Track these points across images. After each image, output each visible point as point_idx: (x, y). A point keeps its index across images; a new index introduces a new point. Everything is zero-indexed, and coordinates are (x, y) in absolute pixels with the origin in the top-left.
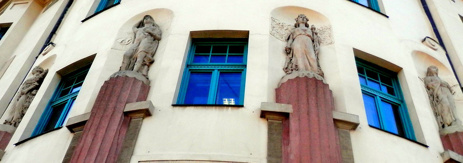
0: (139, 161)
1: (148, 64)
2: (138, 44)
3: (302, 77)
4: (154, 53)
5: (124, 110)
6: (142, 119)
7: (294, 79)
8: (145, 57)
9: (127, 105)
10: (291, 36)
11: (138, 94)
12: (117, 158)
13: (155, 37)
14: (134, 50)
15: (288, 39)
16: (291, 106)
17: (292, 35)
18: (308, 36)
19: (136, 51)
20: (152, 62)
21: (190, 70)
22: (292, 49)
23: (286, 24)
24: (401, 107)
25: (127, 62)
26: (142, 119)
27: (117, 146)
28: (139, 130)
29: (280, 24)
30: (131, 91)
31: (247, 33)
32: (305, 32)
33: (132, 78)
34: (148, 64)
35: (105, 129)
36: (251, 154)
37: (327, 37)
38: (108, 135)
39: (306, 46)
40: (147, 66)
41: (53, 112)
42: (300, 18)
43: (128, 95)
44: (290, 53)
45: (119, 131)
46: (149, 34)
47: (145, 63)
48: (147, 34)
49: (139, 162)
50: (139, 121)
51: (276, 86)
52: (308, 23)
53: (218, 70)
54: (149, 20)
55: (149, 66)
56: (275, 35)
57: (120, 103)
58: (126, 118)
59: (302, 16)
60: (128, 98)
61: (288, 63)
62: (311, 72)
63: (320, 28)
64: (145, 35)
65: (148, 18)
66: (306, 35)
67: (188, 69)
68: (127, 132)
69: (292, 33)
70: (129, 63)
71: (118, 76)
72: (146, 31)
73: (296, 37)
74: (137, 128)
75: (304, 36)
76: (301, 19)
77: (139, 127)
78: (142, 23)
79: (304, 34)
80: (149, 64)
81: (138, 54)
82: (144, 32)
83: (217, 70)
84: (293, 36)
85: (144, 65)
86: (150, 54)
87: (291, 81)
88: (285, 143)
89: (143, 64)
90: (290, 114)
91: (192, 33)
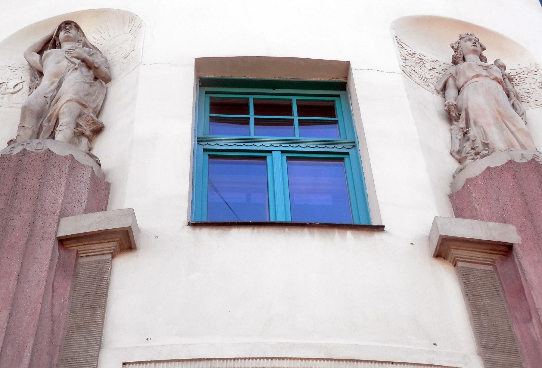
0: (125, 361)
1: (88, 133)
2: (55, 85)
3: (520, 162)
4: (99, 108)
5: (56, 233)
6: (110, 256)
7: (503, 166)
8: (80, 116)
9: (63, 221)
10: (451, 81)
11: (86, 196)
12: (57, 356)
13: (98, 70)
14: (46, 97)
15: (444, 88)
16: (512, 228)
17: (453, 79)
18: (496, 79)
19: (52, 101)
20: (98, 130)
21: (205, 150)
22: (464, 108)
23: (427, 58)
25: (30, 123)
26: (110, 256)
27: (53, 325)
28: (108, 284)
29: (417, 56)
30: (67, 188)
32: (488, 72)
33: (66, 157)
34: (88, 133)
35: (13, 277)
36: (435, 344)
37: (533, 90)
38: (24, 293)
39: (497, 101)
40: (87, 140)
41: (110, 75)
42: (465, 41)
43: (61, 197)
44: (459, 118)
45: (51, 285)
46: (82, 63)
47: (81, 130)
48: (78, 61)
49: (124, 364)
50: (105, 261)
52: (484, 53)
53: (283, 152)
54: (73, 32)
55: (90, 140)
56: (413, 76)
57: (45, 215)
58: (64, 254)
59: (470, 37)
60: (62, 204)
61: (460, 140)
62: (457, 198)
63: (511, 71)
64: (73, 65)
65: (71, 28)
66: (492, 77)
67: (201, 148)
68: (73, 289)
69: (451, 75)
70: (36, 130)
71: (24, 150)
72: (73, 55)
73: (466, 82)
74: (101, 280)
75: (488, 79)
76: (469, 44)
77: (106, 276)
78: (52, 42)
79: (486, 76)
80: (92, 134)
81: (63, 107)
82: (69, 57)
84: (455, 79)
85: (79, 134)
86: (91, 110)
87: (495, 173)
88: (518, 316)
89: (76, 131)
90: (515, 246)
91: (201, 63)
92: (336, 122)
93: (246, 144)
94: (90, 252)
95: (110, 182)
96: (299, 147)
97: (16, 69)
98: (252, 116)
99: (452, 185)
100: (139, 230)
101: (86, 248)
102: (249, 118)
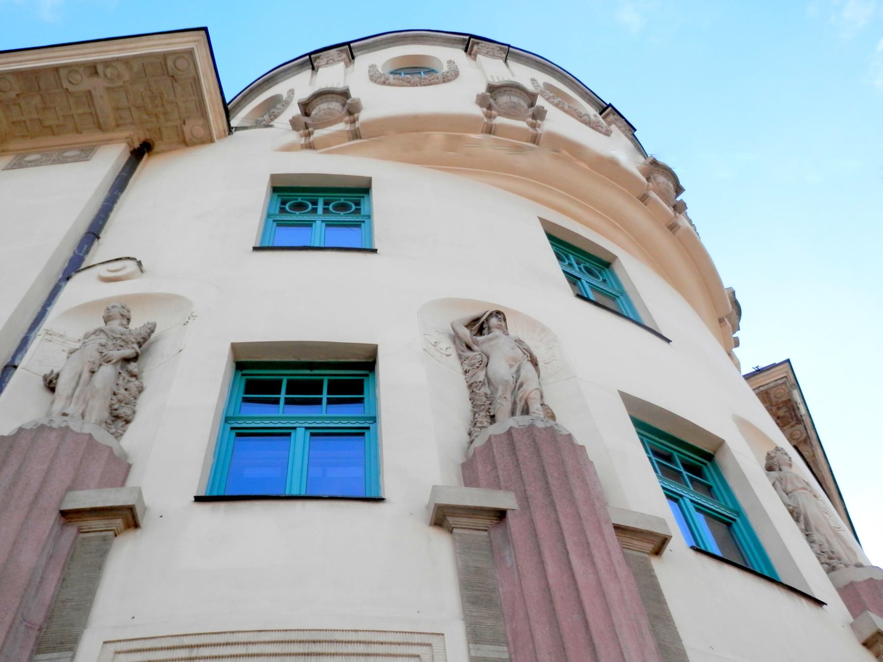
21: (232, 428)
24: (737, 524)
31: (373, 352)
49: (105, 643)
51: (461, 460)
53: (307, 428)
67: (228, 426)
83: (304, 428)
92: (361, 401)
93: (316, 422)
94: (631, 546)
95: (131, 462)
96: (297, 424)
97: (545, 363)
98: (325, 396)
99: (466, 456)
100: (145, 509)
101: (628, 541)
102: (279, 398)
